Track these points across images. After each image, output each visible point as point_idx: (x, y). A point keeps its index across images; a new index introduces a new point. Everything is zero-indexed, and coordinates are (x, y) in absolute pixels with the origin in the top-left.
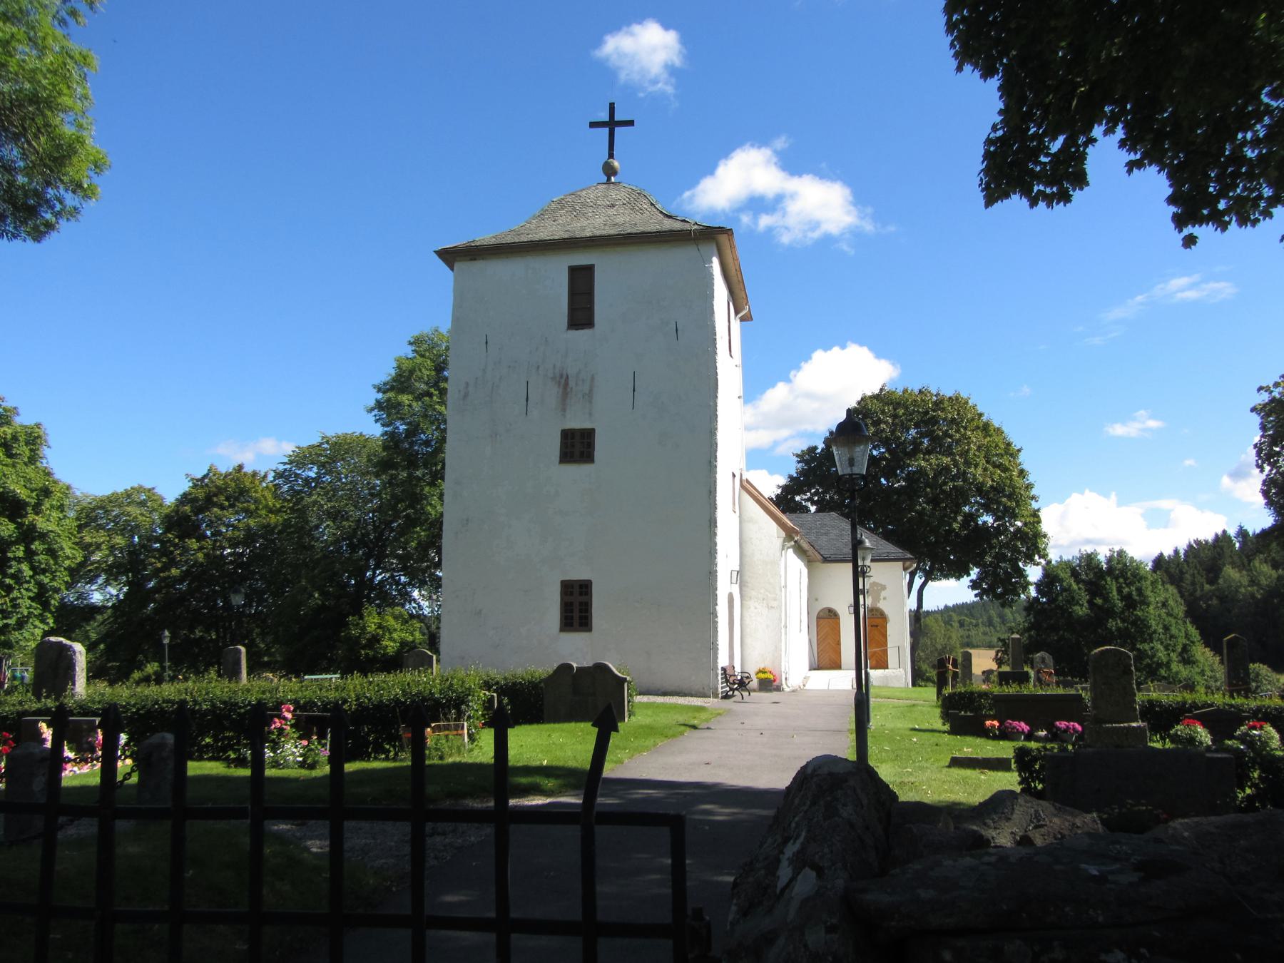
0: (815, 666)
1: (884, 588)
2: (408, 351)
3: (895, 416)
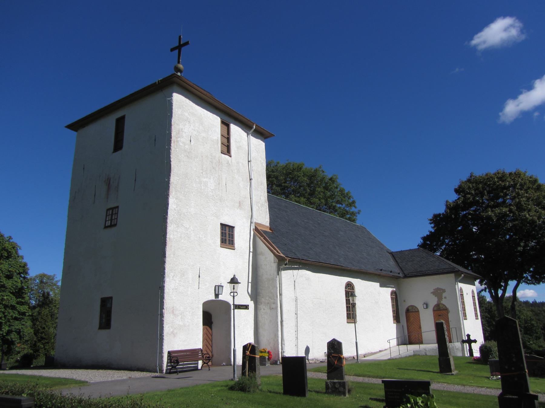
0: (400, 343)
1: (444, 291)
2: (453, 197)
3: (477, 189)
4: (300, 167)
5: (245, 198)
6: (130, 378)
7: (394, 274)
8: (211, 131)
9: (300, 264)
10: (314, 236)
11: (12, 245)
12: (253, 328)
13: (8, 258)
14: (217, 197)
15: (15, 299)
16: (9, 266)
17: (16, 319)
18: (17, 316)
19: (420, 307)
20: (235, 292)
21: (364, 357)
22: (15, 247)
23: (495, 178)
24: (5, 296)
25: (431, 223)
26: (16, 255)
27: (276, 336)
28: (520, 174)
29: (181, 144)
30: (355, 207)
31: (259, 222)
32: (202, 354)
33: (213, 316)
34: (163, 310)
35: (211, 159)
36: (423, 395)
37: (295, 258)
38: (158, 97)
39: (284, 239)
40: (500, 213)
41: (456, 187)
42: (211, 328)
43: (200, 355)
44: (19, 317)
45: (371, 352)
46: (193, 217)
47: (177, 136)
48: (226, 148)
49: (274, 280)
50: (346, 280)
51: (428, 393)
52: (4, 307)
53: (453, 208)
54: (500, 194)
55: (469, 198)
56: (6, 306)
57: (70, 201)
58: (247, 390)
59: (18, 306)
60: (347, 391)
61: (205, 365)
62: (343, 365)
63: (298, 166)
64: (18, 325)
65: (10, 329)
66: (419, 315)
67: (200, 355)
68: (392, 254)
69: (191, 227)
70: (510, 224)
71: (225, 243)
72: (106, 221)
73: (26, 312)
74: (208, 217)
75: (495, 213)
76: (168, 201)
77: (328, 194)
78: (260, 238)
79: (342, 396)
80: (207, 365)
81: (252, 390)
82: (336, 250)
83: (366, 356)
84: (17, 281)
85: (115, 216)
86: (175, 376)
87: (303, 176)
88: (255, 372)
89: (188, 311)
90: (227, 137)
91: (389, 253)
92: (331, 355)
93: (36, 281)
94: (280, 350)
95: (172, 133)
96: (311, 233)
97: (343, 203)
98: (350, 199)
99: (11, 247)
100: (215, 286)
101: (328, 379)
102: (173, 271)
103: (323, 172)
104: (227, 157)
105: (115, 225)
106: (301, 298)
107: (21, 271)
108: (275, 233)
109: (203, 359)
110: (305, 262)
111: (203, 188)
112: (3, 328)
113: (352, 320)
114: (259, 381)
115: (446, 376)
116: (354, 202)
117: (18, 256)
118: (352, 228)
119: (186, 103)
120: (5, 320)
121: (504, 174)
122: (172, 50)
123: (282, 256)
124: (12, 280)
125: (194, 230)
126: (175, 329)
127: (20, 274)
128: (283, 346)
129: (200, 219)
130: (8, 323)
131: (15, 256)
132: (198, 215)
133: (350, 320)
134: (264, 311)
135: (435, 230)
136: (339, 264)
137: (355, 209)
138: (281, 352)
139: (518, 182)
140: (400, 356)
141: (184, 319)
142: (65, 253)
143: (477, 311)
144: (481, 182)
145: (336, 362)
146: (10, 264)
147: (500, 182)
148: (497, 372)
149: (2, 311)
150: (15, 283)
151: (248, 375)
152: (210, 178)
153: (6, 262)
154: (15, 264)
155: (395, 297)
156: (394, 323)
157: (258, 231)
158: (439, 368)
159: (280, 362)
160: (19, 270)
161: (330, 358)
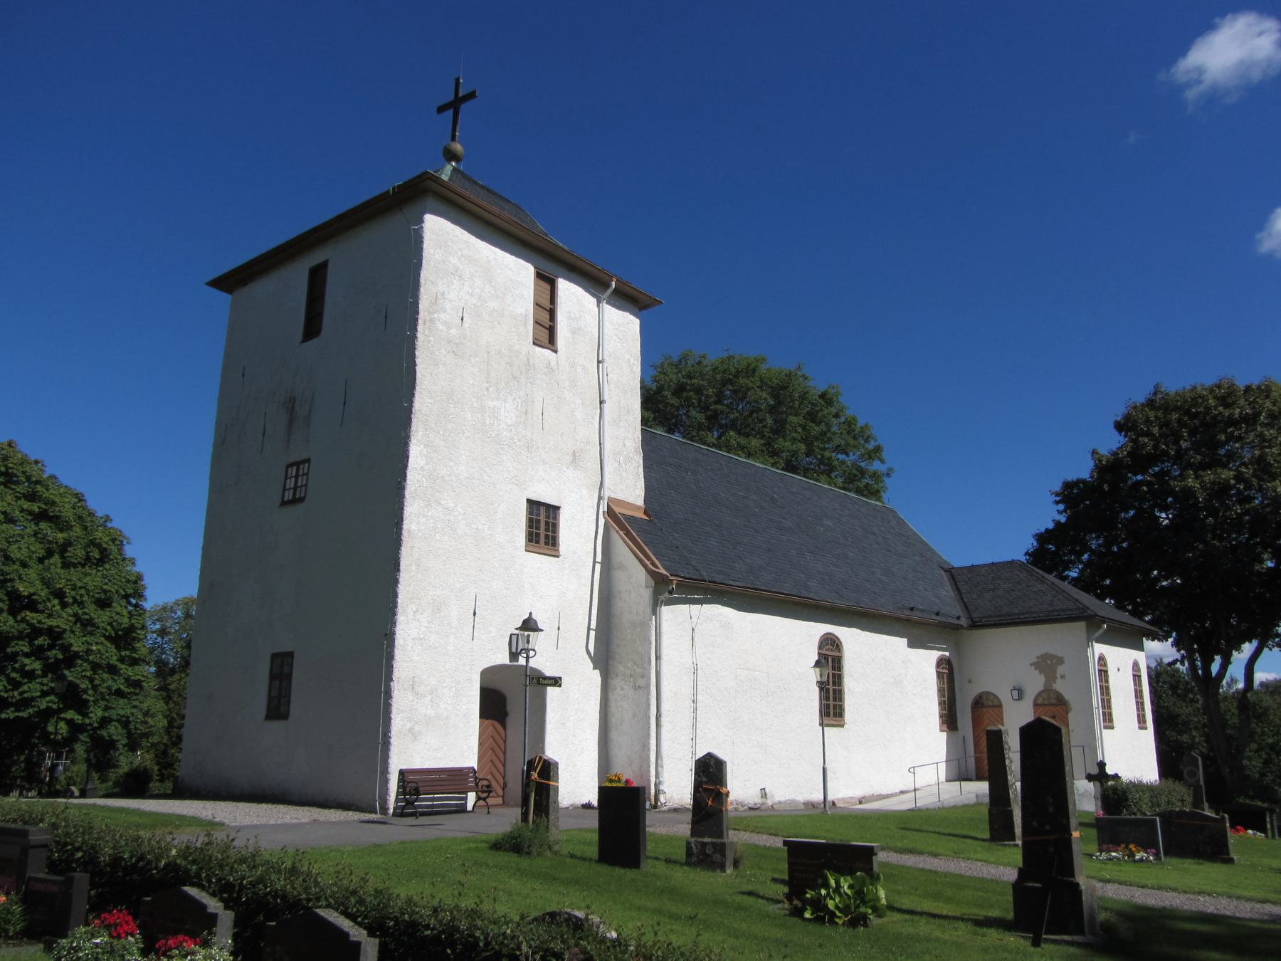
1: (1060, 661)
2: (1111, 442)
4: (751, 368)
5: (588, 443)
6: (315, 821)
7: (944, 619)
8: (512, 295)
9: (705, 591)
10: (755, 529)
11: (110, 535)
12: (597, 728)
13: (102, 561)
14: (520, 441)
15: (115, 651)
16: (103, 580)
17: (119, 693)
18: (122, 687)
19: (1005, 695)
20: (532, 650)
21: (860, 803)
22: (118, 540)
23: (1208, 400)
24: (94, 644)
25: (1057, 503)
26: (119, 557)
27: (646, 747)
28: (1271, 389)
29: (441, 327)
30: (882, 461)
31: (619, 496)
32: (476, 779)
33: (508, 701)
34: (392, 684)
35: (510, 357)
36: (858, 873)
37: (694, 577)
38: (387, 227)
39: (677, 535)
40: (1213, 483)
41: (1119, 419)
42: (504, 726)
43: (471, 782)
44: (126, 690)
45: (878, 794)
46: (464, 486)
47: (431, 309)
48: (547, 332)
49: (644, 625)
50: (822, 629)
51: (869, 870)
52: (92, 667)
53: (1109, 469)
54: (1219, 437)
55: (1145, 445)
56: (95, 667)
57: (215, 446)
58: (526, 850)
59: (123, 666)
60: (729, 863)
61: (481, 803)
62: (724, 809)
63: (749, 365)
64: (125, 707)
65: (107, 715)
66: (1002, 714)
67: (471, 782)
68: (952, 573)
69: (459, 505)
70: (1237, 509)
71: (537, 542)
72: (285, 490)
73: (144, 681)
74: (498, 486)
75: (1203, 481)
76: (408, 450)
77: (816, 430)
78: (617, 532)
79: (718, 872)
80: (484, 802)
81: (534, 850)
82: (804, 561)
83: (863, 800)
84: (120, 612)
85: (302, 479)
86: (411, 821)
87: (760, 387)
88: (547, 815)
89: (446, 687)
90: (549, 309)
91: (945, 571)
92: (702, 787)
93: (176, 613)
94: (653, 780)
95: (420, 302)
96: (749, 522)
97: (848, 451)
98: (869, 442)
99: (108, 538)
100: (511, 635)
101: (693, 833)
102: (415, 600)
103: (806, 378)
104: (547, 352)
105: (302, 500)
106: (708, 665)
107: (130, 591)
108: (656, 521)
109: (477, 790)
110: (716, 587)
111: (488, 422)
112: (91, 712)
113: (832, 720)
114: (554, 834)
115: (999, 847)
116: (878, 449)
117: (124, 559)
118: (858, 510)
119: (454, 236)
120: (94, 696)
121: (1232, 390)
122: (441, 110)
123: (661, 574)
124: (110, 611)
125: (465, 513)
126: (417, 723)
127: (126, 597)
128: (660, 769)
129: (480, 490)
130: (103, 703)
131: (116, 559)
132: (474, 481)
133: (828, 720)
134: (622, 693)
135: (1068, 518)
136: (804, 593)
137: (882, 465)
138: (656, 782)
139: (1264, 408)
140: (939, 805)
141: (436, 703)
142: (203, 556)
143: (1143, 709)
144: (1176, 409)
145: (710, 802)
146: (106, 575)
147: (1221, 408)
148: (1112, 844)
149: (88, 677)
150: (116, 618)
151: (533, 822)
152: (506, 400)
153: (99, 571)
154: (116, 577)
155: (947, 671)
156: (941, 731)
157: (615, 517)
158: (988, 833)
159: (650, 804)
160: (124, 590)
161: (699, 792)
